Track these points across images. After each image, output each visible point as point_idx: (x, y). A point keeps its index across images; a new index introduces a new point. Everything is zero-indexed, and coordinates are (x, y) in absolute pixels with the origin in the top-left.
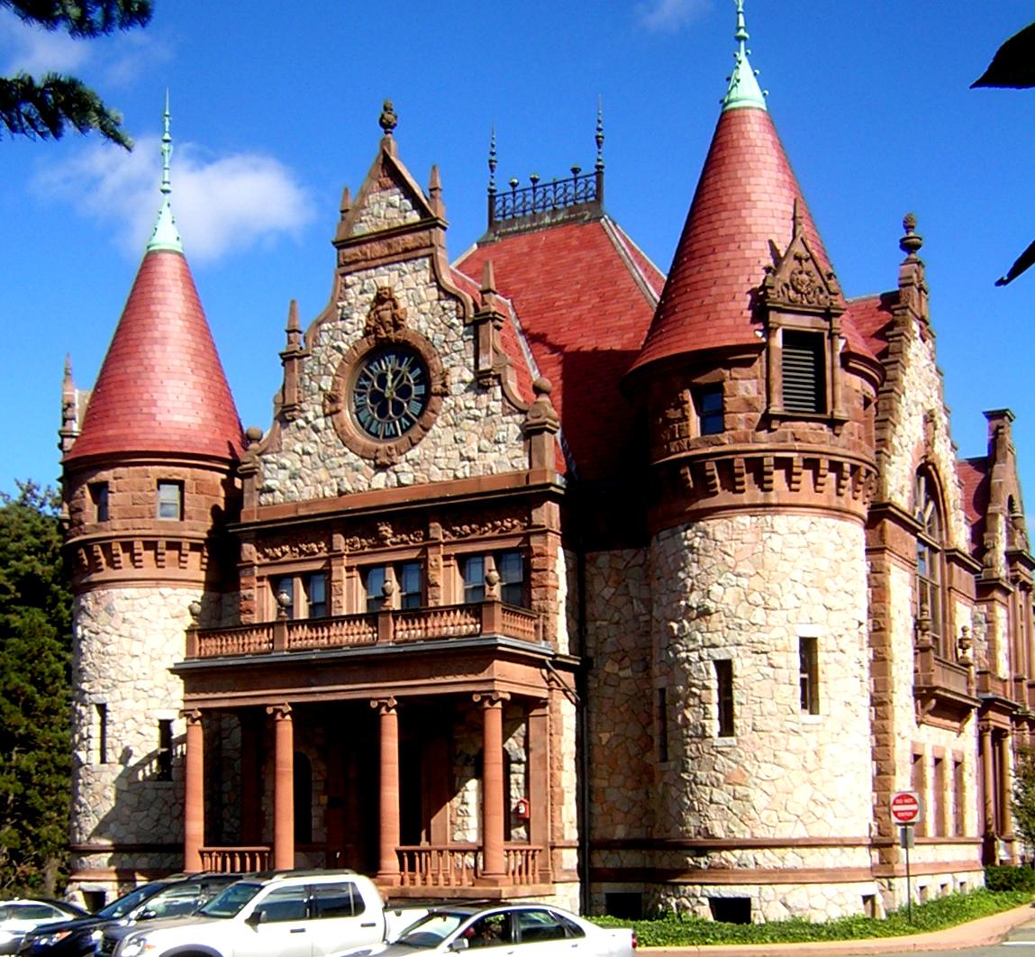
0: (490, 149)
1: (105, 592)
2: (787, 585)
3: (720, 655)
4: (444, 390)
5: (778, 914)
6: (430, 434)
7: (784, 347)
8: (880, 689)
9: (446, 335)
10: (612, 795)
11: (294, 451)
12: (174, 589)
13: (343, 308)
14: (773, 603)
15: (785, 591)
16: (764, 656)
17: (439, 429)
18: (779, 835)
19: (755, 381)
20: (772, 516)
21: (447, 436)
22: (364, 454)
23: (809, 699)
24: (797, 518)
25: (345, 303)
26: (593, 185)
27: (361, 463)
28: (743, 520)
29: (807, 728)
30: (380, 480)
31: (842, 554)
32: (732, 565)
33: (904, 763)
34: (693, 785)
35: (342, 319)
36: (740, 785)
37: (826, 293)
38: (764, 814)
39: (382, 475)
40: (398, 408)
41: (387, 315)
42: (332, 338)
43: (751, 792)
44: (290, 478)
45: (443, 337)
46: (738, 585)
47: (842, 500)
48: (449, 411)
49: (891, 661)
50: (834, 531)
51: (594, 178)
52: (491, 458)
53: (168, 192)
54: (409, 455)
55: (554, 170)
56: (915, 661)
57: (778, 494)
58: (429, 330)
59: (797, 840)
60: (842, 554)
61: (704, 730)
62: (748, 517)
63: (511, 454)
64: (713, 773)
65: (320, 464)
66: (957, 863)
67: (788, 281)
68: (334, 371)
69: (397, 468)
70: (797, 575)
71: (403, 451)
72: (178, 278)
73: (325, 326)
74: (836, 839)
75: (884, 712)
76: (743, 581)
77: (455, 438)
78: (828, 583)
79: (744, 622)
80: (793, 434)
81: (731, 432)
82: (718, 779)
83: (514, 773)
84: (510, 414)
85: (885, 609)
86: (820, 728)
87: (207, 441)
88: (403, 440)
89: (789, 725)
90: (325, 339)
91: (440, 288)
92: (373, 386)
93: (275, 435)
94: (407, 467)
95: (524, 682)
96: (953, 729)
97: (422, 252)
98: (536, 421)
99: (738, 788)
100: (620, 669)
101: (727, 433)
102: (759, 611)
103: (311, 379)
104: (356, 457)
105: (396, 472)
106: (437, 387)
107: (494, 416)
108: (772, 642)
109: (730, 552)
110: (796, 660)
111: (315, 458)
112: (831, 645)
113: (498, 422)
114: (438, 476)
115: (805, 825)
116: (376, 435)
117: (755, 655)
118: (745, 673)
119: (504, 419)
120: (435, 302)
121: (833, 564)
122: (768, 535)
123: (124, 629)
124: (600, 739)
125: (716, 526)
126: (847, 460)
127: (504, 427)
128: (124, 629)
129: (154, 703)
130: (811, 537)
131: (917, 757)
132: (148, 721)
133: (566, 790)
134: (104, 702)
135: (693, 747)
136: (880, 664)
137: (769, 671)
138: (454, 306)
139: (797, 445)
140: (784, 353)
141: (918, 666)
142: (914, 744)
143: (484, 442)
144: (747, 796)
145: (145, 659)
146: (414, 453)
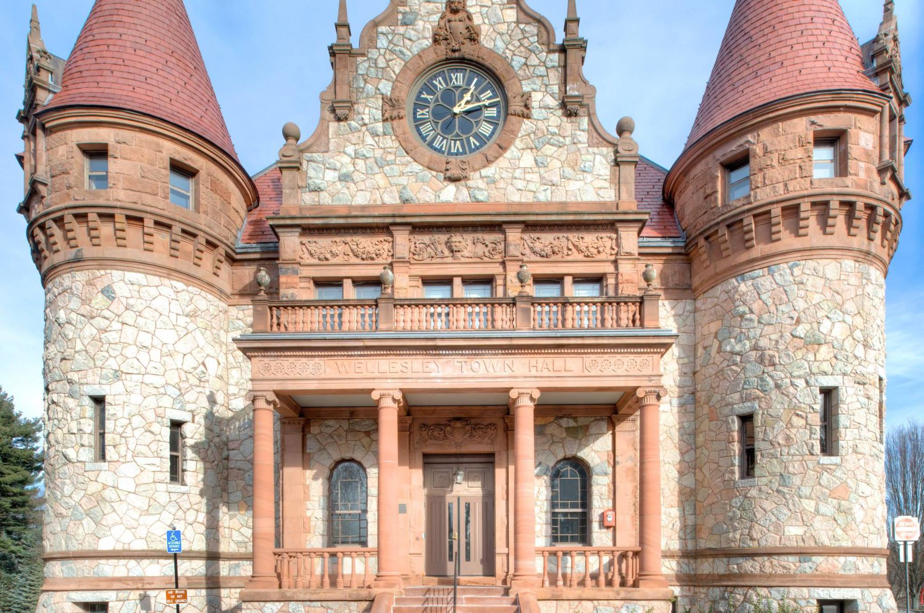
1: (102, 272)
3: (828, 382)
4: (526, 111)
6: (508, 154)
9: (526, 58)
11: (345, 153)
12: (188, 286)
13: (404, 14)
21: (528, 160)
22: (432, 165)
25: (407, 9)
27: (428, 174)
30: (450, 194)
32: (841, 303)
34: (796, 498)
35: (405, 24)
36: (844, 500)
38: (862, 526)
39: (451, 188)
41: (460, 27)
42: (390, 42)
44: (340, 180)
48: (529, 135)
52: (573, 186)
54: (484, 172)
58: (507, 51)
64: (819, 487)
65: (376, 169)
68: (394, 77)
69: (470, 183)
71: (477, 166)
76: (848, 319)
77: (536, 161)
79: (850, 355)
81: (854, 177)
83: (597, 484)
84: (598, 145)
88: (477, 157)
90: (382, 42)
93: (321, 133)
94: (481, 184)
98: (627, 153)
99: (843, 502)
102: (861, 347)
103: (366, 81)
104: (421, 167)
105: (468, 188)
107: (579, 146)
111: (370, 162)
113: (583, 151)
114: (516, 198)
117: (857, 385)
119: (590, 150)
120: (513, 25)
123: (129, 317)
127: (590, 157)
128: (129, 317)
129: (166, 401)
132: (159, 419)
134: (103, 393)
138: (536, 32)
143: (568, 171)
145: (155, 354)
146: (488, 171)
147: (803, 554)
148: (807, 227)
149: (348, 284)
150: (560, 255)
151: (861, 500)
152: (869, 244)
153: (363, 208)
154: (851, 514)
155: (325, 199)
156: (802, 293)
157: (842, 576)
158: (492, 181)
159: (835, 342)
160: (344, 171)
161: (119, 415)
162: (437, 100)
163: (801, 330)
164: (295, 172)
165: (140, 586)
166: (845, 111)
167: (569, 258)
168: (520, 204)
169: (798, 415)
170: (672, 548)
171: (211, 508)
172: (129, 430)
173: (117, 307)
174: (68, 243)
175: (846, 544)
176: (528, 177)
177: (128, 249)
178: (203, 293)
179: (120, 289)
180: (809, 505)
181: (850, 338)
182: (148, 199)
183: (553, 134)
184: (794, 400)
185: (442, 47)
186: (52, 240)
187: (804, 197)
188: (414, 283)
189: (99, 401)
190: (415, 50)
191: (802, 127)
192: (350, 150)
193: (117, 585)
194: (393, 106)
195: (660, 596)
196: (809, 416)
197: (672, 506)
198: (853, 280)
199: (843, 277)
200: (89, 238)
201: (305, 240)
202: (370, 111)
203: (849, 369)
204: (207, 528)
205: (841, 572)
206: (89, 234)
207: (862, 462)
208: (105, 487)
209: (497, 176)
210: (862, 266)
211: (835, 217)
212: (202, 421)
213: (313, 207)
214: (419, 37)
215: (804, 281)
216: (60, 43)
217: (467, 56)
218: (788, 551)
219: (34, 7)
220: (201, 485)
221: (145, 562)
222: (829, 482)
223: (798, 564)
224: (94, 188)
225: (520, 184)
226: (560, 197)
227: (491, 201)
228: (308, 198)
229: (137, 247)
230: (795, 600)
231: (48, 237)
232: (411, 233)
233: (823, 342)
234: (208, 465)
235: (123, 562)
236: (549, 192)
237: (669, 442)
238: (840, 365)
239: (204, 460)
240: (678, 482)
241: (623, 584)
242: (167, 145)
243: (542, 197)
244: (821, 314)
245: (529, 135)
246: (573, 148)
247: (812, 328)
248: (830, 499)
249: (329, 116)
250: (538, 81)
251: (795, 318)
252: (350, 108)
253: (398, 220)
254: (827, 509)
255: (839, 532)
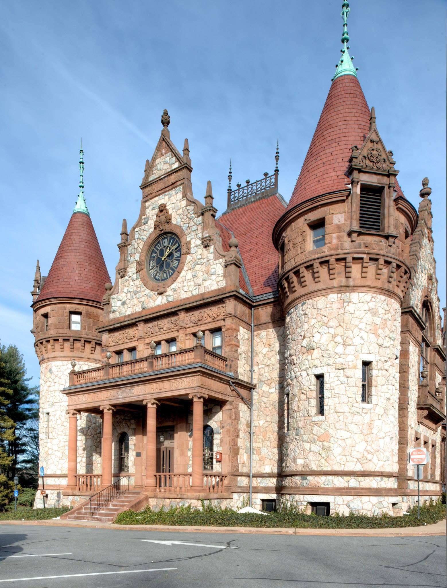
0: (229, 167)
2: (356, 331)
3: (318, 371)
4: (188, 251)
5: (344, 512)
6: (181, 275)
7: (361, 194)
8: (401, 402)
10: (264, 451)
14: (349, 341)
15: (355, 335)
16: (342, 371)
17: (186, 274)
18: (346, 469)
19: (344, 214)
20: (350, 293)
23: (365, 397)
24: (363, 294)
26: (273, 180)
28: (333, 297)
29: (364, 411)
31: (389, 316)
32: (326, 322)
33: (412, 441)
36: (327, 442)
37: (388, 163)
38: (338, 458)
39: (160, 297)
40: (168, 265)
42: (139, 234)
43: (332, 445)
45: (187, 225)
46: (329, 333)
47: (391, 286)
48: (190, 262)
49: (408, 388)
50: (385, 303)
51: (274, 177)
52: (207, 283)
53: (83, 187)
55: (256, 176)
56: (419, 392)
57: (354, 280)
59: (357, 472)
60: (389, 316)
61: (308, 413)
62: (336, 294)
63: (218, 280)
64: (312, 435)
65: (134, 296)
66: (432, 491)
67: (366, 155)
68: (140, 250)
69: (167, 294)
70: (362, 326)
72: (85, 224)
73: (137, 229)
74: (379, 472)
75: (404, 414)
76: (332, 331)
78: (380, 331)
79: (331, 353)
80: (364, 244)
81: (329, 245)
82: (314, 439)
83: (216, 439)
85: (406, 362)
86: (372, 411)
87: (93, 295)
89: (354, 409)
91: (187, 199)
92: (157, 256)
95: (217, 391)
96: (432, 429)
97: (179, 183)
98: (229, 259)
99: (325, 443)
100: (270, 388)
101: (327, 245)
102: (341, 347)
103: (131, 256)
105: (166, 296)
106: (184, 250)
108: (347, 363)
109: (325, 315)
110: (359, 374)
112: (380, 365)
113: (212, 264)
115: (361, 464)
116: (158, 280)
117: (337, 371)
118: (331, 380)
119: (215, 262)
121: (383, 321)
122: (347, 304)
123: (57, 380)
124: (259, 423)
125: (320, 302)
126: (395, 261)
127: (214, 266)
130: (371, 305)
131: (417, 439)
133: (240, 448)
135: (302, 422)
136: (404, 387)
137: (345, 379)
138: (193, 209)
139: (366, 250)
140: (361, 197)
141: (420, 394)
142: (416, 433)
144: (329, 447)
147: (304, 475)
148: (305, 281)
149: (125, 352)
150: (202, 321)
151: (340, 442)
152: (347, 281)
153: (129, 316)
154: (331, 451)
155: (117, 315)
156: (306, 319)
157: (323, 488)
158: (175, 290)
159: (322, 347)
160: (123, 300)
161: (53, 420)
162: (157, 256)
163: (304, 343)
164: (107, 305)
165: (58, 488)
166: (322, 207)
167: (206, 322)
168: (186, 299)
169: (303, 393)
170: (274, 471)
171: (89, 456)
172: (56, 426)
173: (53, 376)
174: (314, 280)
175: (328, 469)
176: (189, 284)
177: (56, 353)
178: (86, 363)
179: (54, 369)
180: (307, 446)
181: (333, 343)
182: (61, 331)
183: (199, 259)
184: (302, 384)
185: (158, 230)
186: (292, 285)
187: (300, 265)
188: (188, 337)
189: (48, 414)
190: (148, 235)
191: (301, 223)
192: (125, 290)
193: (52, 488)
194: (140, 265)
195: (194, 497)
196: (308, 392)
197: (275, 447)
198: (336, 306)
199: (328, 306)
200: (328, 275)
201: (110, 335)
202: (132, 270)
203: (331, 362)
204: (87, 464)
205: (322, 486)
206: (329, 272)
207: (341, 418)
208: (49, 449)
209: (177, 287)
210: (344, 295)
211: (318, 272)
212: (85, 418)
213: (113, 320)
214: (148, 230)
215: (307, 313)
216: (45, 272)
217: (166, 231)
218: (296, 474)
219: (38, 261)
220: (84, 446)
221: (61, 479)
222: (317, 432)
223: (301, 481)
224: (315, 248)
225: (186, 289)
226: (202, 291)
227: (175, 300)
228: (112, 316)
229: (58, 351)
230: (296, 502)
231: (289, 284)
232: (186, 313)
233: (315, 347)
234: (88, 437)
235: (53, 478)
236: (197, 289)
237: (274, 410)
238: (325, 359)
239: (85, 435)
240: (278, 433)
241: (221, 492)
242: (68, 306)
243: (195, 293)
244: (315, 330)
245: (190, 262)
246: (207, 263)
247: (310, 340)
248: (318, 442)
249: (119, 276)
250: (193, 234)
251: (303, 335)
252: (125, 272)
253: (138, 320)
254: (316, 448)
255: (323, 461)
